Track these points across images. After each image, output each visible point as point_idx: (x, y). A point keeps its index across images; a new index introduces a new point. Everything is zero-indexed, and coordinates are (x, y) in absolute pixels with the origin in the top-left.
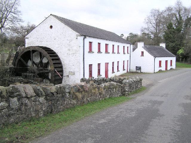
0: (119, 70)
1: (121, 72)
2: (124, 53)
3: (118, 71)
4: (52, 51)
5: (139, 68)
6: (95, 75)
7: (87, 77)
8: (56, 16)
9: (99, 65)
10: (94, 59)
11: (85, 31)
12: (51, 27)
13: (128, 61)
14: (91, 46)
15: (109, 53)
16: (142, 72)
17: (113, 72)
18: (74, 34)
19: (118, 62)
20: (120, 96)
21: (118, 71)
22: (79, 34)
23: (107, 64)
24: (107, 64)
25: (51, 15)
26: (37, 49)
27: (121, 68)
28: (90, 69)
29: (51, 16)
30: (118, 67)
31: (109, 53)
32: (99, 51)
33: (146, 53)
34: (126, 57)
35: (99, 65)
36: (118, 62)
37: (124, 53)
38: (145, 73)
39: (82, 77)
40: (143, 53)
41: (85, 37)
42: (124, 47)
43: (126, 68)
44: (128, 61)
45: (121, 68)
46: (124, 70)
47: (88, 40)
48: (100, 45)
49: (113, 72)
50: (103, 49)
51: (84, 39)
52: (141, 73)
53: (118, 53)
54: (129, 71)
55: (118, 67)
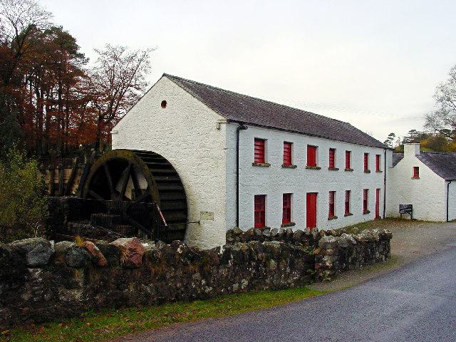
0: (351, 211)
1: (357, 217)
2: (367, 171)
3: (348, 213)
4: (165, 160)
5: (409, 209)
6: (274, 220)
7: (248, 223)
8: (176, 78)
9: (287, 198)
10: (272, 182)
11: (238, 111)
12: (164, 104)
13: (378, 190)
14: (333, 158)
15: (268, 166)
16: (415, 220)
17: (332, 215)
18: (213, 117)
19: (348, 192)
20: (297, 282)
21: (348, 213)
22: (223, 118)
23: (312, 198)
24: (312, 198)
25: (164, 75)
26: (130, 159)
27: (357, 206)
28: (285, 204)
29: (165, 78)
30: (347, 204)
31: (319, 168)
32: (332, 167)
33: (425, 170)
34: (374, 181)
35: (287, 198)
36: (348, 192)
37: (367, 171)
38: (422, 221)
39: (232, 225)
40: (416, 169)
41: (242, 126)
42: (366, 155)
43: (371, 207)
44: (378, 190)
45: (357, 206)
46: (366, 211)
47: (250, 135)
48: (333, 154)
49: (332, 215)
50: (300, 156)
51: (238, 132)
52: (414, 220)
53: (348, 168)
54: (381, 215)
55: (347, 204)
